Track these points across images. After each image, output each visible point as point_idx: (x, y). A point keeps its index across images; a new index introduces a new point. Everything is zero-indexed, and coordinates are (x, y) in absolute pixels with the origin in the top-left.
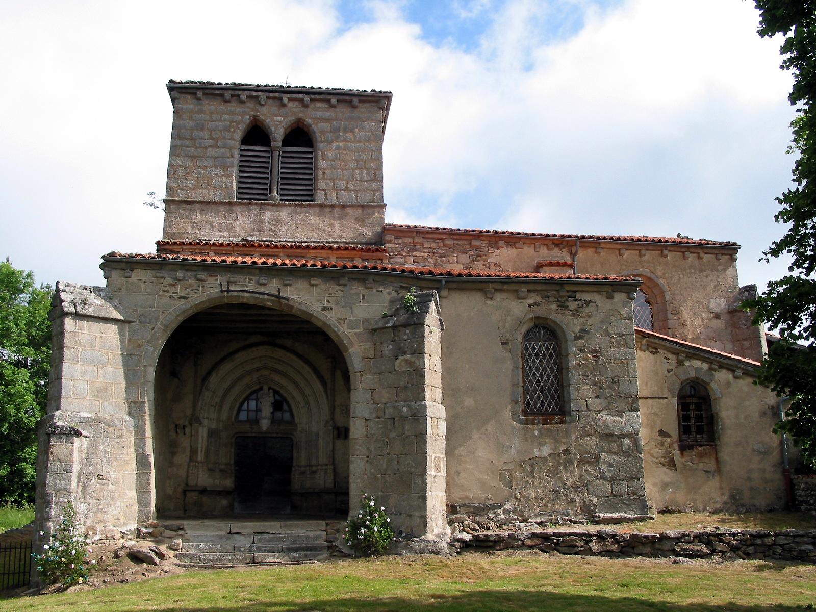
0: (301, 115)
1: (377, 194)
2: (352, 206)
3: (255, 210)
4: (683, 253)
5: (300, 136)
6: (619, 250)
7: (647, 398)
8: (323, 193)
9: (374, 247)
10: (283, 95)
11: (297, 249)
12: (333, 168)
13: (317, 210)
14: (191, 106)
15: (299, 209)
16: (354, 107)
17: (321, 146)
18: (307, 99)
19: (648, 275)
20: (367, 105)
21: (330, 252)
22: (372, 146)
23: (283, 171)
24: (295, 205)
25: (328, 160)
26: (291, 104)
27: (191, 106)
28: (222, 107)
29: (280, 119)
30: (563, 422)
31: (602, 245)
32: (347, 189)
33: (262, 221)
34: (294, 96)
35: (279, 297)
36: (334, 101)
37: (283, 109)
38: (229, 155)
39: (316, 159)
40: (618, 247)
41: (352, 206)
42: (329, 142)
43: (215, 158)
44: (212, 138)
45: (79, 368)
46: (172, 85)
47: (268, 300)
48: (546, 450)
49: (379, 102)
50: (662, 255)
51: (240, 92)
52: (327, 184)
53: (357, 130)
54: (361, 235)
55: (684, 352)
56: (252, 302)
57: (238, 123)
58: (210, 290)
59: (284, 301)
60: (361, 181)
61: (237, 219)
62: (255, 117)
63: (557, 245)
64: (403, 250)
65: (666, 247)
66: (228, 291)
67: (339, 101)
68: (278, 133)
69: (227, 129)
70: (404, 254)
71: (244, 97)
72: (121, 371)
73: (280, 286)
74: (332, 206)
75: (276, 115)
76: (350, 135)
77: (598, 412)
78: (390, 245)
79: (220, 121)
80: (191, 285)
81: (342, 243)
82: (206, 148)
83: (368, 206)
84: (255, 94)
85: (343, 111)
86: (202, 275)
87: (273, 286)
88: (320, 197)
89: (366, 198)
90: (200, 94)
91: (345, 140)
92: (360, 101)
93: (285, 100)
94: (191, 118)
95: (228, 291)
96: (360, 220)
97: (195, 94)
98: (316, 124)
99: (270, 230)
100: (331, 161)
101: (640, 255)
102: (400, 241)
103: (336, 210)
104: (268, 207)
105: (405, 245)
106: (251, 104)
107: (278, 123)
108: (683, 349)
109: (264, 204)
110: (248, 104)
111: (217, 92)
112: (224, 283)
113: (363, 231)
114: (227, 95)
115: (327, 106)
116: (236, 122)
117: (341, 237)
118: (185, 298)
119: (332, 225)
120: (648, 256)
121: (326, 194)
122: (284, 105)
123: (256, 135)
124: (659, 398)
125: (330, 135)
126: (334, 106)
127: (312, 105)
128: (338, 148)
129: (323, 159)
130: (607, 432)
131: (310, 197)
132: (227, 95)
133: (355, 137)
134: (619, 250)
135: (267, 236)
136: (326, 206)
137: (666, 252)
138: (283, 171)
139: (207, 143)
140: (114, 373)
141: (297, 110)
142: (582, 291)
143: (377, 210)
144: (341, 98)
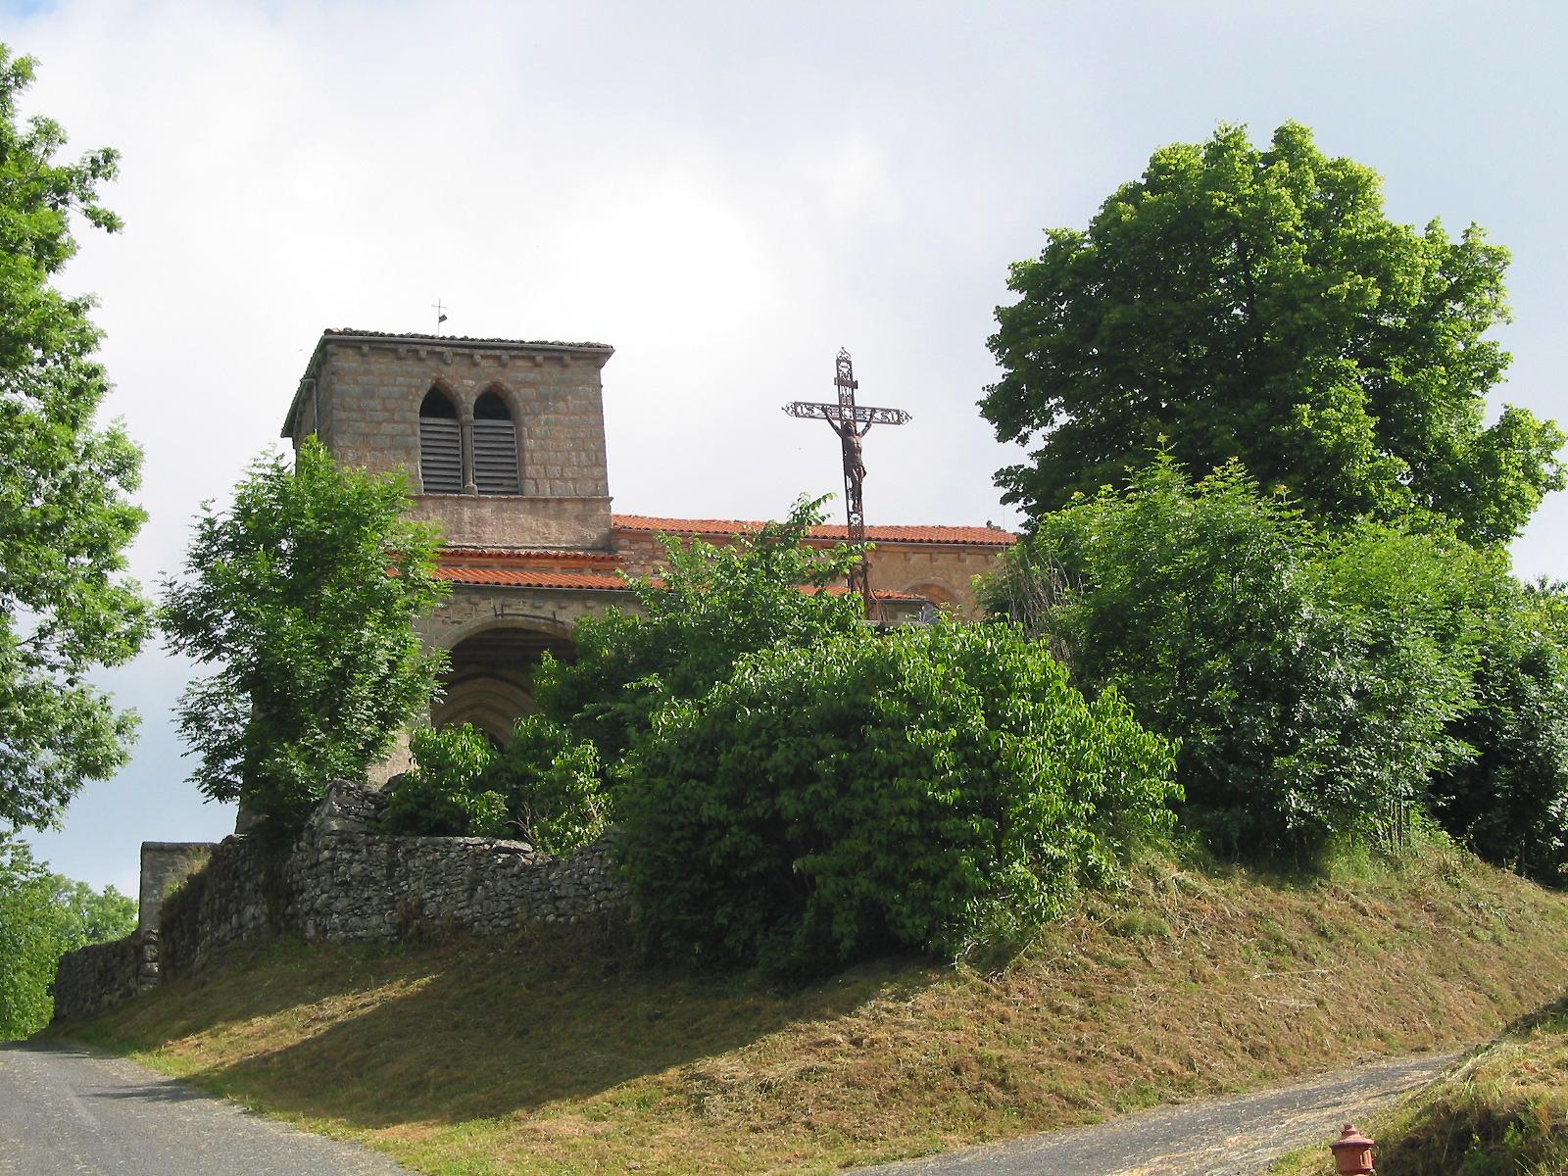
0: (498, 378)
1: (600, 484)
2: (572, 500)
3: (450, 506)
4: (986, 556)
5: (494, 405)
6: (905, 553)
8: (533, 482)
9: (602, 554)
10: (475, 351)
11: (512, 559)
12: (542, 448)
13: (527, 505)
14: (354, 365)
15: (505, 505)
16: (566, 366)
17: (526, 419)
18: (505, 356)
19: (942, 585)
20: (581, 363)
21: (554, 561)
22: (592, 419)
23: (477, 452)
24: (500, 500)
25: (537, 438)
26: (484, 363)
27: (354, 365)
28: (396, 366)
29: (471, 383)
31: (884, 548)
32: (562, 478)
33: (460, 520)
34: (489, 352)
35: (554, 620)
36: (539, 358)
37: (474, 370)
38: (409, 432)
39: (520, 436)
40: (905, 550)
41: (572, 500)
42: (536, 414)
43: (393, 437)
44: (386, 410)
46: (330, 336)
47: (544, 624)
49: (595, 356)
50: (960, 560)
51: (418, 347)
52: (538, 471)
53: (570, 398)
54: (583, 538)
56: (526, 627)
57: (418, 388)
58: (485, 613)
59: (559, 625)
60: (579, 466)
61: (428, 518)
64: (641, 559)
65: (963, 549)
66: (502, 615)
67: (545, 358)
68: (468, 400)
69: (404, 396)
70: (642, 562)
71: (423, 354)
73: (555, 609)
74: (547, 501)
75: (465, 378)
76: (561, 405)
78: (625, 552)
79: (394, 385)
80: (464, 609)
81: (562, 548)
82: (380, 423)
83: (591, 500)
84: (438, 349)
85: (552, 372)
86: (475, 598)
87: (548, 609)
88: (530, 488)
89: (586, 489)
90: (366, 349)
91: (556, 412)
93: (477, 357)
94: (356, 382)
95: (502, 615)
96: (582, 519)
97: (360, 348)
99: (472, 532)
100: (540, 435)
101: (932, 560)
102: (637, 546)
103: (552, 505)
104: (466, 502)
105: (643, 552)
106: (432, 363)
107: (467, 388)
109: (461, 498)
110: (429, 362)
111: (387, 346)
112: (498, 607)
113: (586, 532)
114: (402, 349)
115: (530, 364)
116: (415, 387)
117: (559, 541)
118: (459, 623)
119: (547, 526)
120: (942, 560)
121: (536, 483)
123: (438, 403)
125: (536, 405)
127: (511, 364)
128: (547, 422)
129: (530, 437)
131: (517, 490)
133: (568, 407)
134: (905, 553)
135: (468, 540)
136: (538, 500)
137: (963, 555)
138: (477, 452)
139: (381, 416)
141: (491, 370)
143: (601, 504)
144: (549, 354)
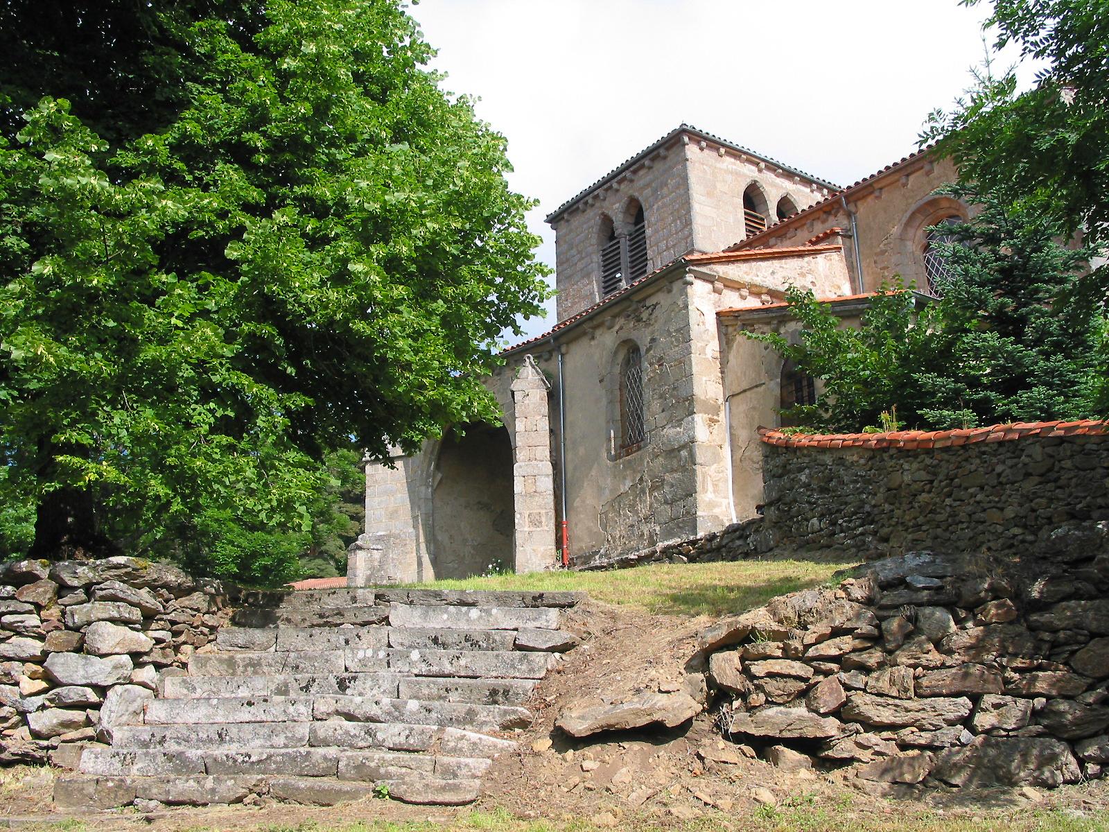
0: (631, 192)
7: (745, 391)
16: (665, 158)
20: (674, 149)
26: (622, 186)
29: (617, 205)
30: (639, 448)
45: (377, 500)
48: (628, 483)
55: (773, 318)
62: (603, 214)
63: (828, 213)
72: (407, 495)
76: (665, 190)
77: (663, 427)
92: (667, 149)
98: (641, 194)
108: (771, 315)
122: (617, 191)
124: (757, 386)
126: (650, 168)
130: (669, 448)
132: (581, 205)
140: (401, 498)
142: (649, 296)
144: (651, 156)
